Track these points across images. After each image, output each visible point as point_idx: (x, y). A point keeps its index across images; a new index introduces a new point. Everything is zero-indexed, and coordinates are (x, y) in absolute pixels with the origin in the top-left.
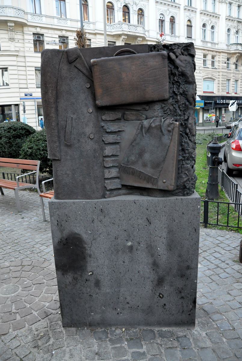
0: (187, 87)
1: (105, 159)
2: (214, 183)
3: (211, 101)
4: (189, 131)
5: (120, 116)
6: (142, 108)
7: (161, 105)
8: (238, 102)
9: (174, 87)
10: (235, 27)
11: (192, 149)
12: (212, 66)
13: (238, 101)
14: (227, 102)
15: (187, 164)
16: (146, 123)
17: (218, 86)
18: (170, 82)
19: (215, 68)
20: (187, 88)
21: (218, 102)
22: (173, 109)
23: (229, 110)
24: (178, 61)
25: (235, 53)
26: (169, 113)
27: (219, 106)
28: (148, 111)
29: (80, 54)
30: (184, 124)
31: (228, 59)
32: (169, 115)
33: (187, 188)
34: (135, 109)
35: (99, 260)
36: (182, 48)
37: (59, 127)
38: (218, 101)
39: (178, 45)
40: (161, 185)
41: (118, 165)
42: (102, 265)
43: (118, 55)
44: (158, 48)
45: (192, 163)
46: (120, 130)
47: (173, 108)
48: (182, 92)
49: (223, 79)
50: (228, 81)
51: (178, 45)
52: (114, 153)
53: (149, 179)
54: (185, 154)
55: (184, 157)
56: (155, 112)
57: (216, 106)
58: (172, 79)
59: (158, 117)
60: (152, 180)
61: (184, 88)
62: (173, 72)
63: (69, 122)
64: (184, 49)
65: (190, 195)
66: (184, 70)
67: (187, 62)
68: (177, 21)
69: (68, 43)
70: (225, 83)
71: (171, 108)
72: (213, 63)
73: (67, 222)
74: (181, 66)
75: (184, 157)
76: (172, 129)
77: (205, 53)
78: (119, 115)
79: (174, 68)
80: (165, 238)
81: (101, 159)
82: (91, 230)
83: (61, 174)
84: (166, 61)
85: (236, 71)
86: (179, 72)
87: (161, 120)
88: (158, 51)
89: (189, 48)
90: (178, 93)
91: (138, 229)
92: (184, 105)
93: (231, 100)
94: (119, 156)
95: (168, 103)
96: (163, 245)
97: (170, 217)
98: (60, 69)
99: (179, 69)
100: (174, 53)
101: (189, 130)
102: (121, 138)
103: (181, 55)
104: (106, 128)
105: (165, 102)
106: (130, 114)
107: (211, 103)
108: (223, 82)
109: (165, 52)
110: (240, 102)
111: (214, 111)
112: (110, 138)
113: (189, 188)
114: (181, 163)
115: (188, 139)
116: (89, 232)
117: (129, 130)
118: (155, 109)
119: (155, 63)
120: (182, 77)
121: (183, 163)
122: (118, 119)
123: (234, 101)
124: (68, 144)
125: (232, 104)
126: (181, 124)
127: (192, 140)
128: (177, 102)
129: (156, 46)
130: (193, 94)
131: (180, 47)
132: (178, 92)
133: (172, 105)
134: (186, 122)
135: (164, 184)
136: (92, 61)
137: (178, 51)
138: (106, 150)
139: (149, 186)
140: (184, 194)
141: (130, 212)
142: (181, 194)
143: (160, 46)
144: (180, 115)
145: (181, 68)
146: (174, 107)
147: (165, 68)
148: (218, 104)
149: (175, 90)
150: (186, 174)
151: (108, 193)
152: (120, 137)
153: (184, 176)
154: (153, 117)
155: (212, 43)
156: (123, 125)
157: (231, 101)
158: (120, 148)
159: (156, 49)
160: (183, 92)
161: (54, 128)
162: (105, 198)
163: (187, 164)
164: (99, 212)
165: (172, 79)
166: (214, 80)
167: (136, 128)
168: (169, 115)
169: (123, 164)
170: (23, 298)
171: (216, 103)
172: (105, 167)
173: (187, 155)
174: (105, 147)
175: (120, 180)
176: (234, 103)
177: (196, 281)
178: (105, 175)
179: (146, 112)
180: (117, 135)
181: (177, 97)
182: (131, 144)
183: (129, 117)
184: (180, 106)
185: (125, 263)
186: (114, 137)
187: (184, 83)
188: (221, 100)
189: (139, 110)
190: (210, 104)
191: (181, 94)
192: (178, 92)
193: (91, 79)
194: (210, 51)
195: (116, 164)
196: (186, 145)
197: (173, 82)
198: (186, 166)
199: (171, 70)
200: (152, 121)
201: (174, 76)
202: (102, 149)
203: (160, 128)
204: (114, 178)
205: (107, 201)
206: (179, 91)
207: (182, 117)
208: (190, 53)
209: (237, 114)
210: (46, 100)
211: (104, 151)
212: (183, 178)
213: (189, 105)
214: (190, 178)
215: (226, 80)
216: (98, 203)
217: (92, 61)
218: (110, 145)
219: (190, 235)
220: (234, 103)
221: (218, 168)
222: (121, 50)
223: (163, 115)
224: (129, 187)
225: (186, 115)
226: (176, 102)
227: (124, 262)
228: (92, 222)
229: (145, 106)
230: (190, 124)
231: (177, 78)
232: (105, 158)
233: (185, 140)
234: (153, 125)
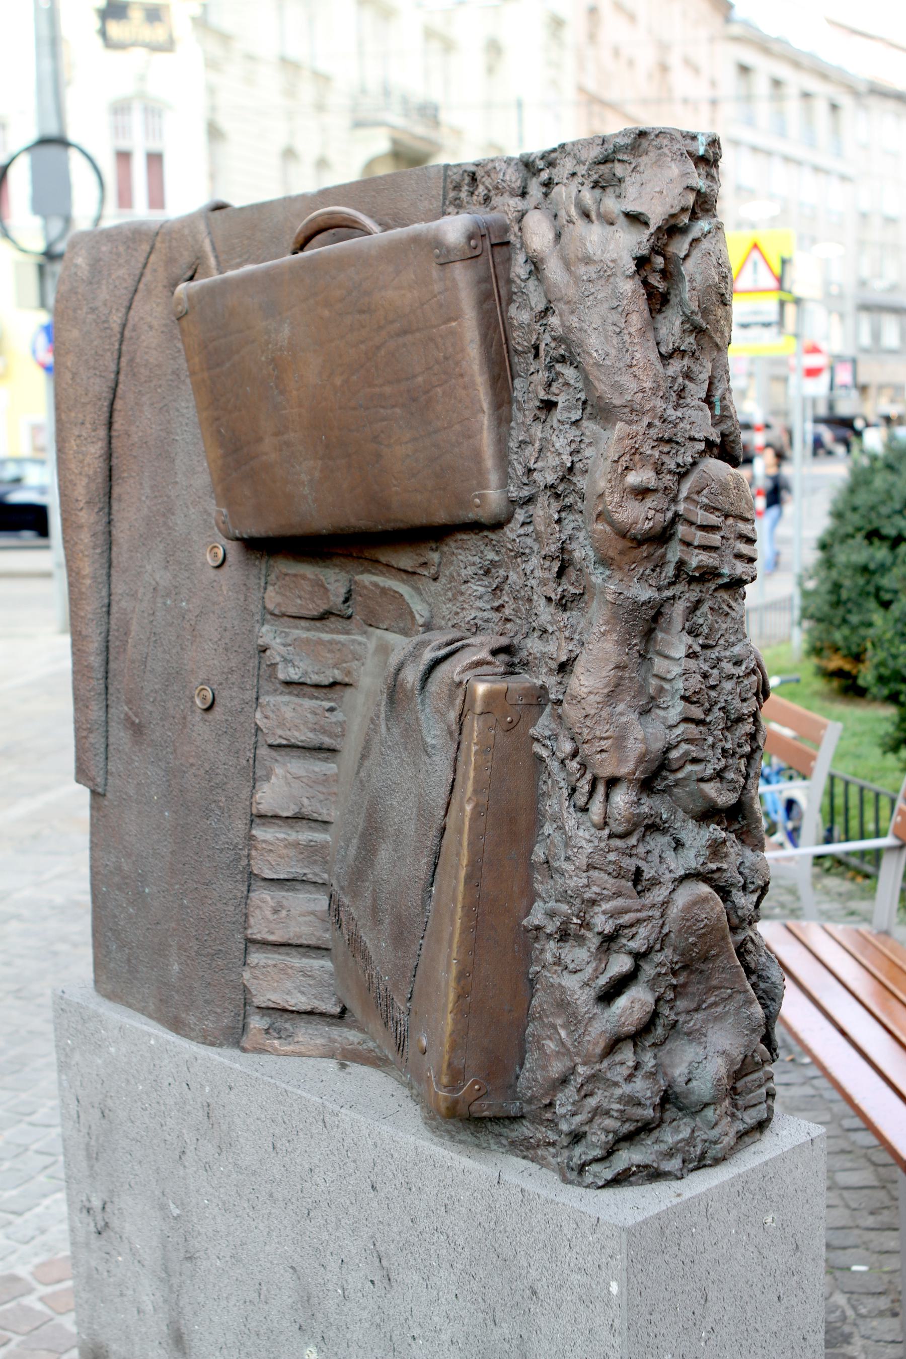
52: (308, 808)
78: (334, 580)
81: (240, 825)
104: (278, 659)
129: (480, 173)
151: (257, 1023)
195: (317, 869)
223: (486, 615)
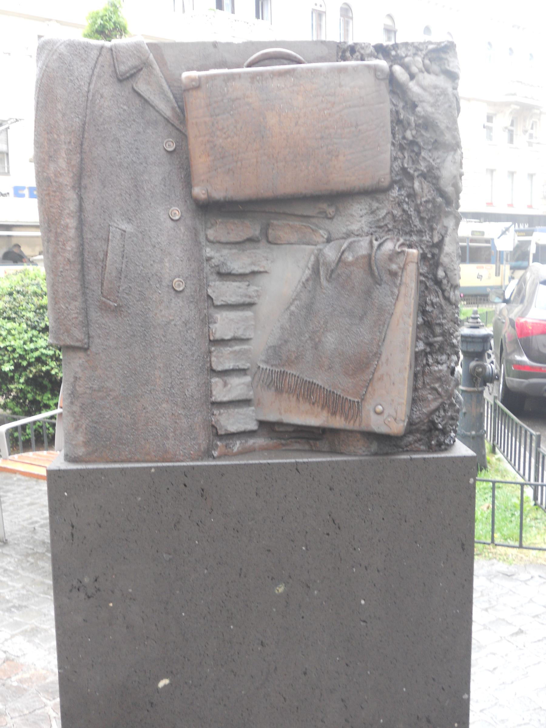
0: (438, 158)
2: (473, 433)
4: (443, 274)
9: (405, 157)
11: (452, 323)
13: (517, 224)
16: (330, 253)
22: (402, 215)
24: (413, 86)
26: (390, 226)
29: (148, 58)
30: (429, 256)
31: (490, 119)
32: (389, 230)
33: (437, 429)
34: (300, 213)
36: (426, 55)
37: (86, 256)
41: (248, 365)
42: (200, 655)
44: (362, 52)
46: (256, 269)
47: (400, 213)
48: (425, 170)
53: (333, 403)
54: (435, 336)
55: (430, 345)
56: (352, 223)
58: (400, 137)
60: (347, 406)
61: (431, 161)
62: (402, 117)
65: (446, 450)
67: (438, 91)
68: (356, 12)
71: (395, 212)
73: (100, 526)
74: (423, 101)
75: (430, 345)
78: (254, 230)
80: (378, 571)
84: (384, 88)
86: (417, 116)
88: (362, 59)
89: (443, 56)
90: (416, 174)
91: (306, 546)
92: (430, 206)
94: (252, 342)
95: (388, 200)
98: (91, 94)
99: (419, 109)
101: (445, 272)
102: (257, 291)
103: (422, 72)
105: (381, 197)
106: (283, 230)
109: (383, 63)
114: (422, 361)
118: (354, 213)
121: (427, 360)
122: (251, 240)
124: (111, 303)
126: (423, 257)
128: (412, 195)
130: (455, 177)
131: (420, 53)
132: (415, 171)
133: (399, 204)
134: (436, 251)
136: (185, 75)
138: (215, 323)
139: (338, 422)
140: (431, 445)
142: (422, 447)
143: (367, 47)
145: (423, 107)
146: (404, 210)
147: (382, 105)
149: (406, 165)
152: (256, 288)
153: (430, 397)
156: (263, 257)
159: (357, 54)
160: (429, 171)
165: (399, 136)
168: (389, 230)
173: (440, 339)
176: (507, 229)
178: (214, 393)
179: (327, 222)
180: (247, 283)
181: (413, 184)
182: (288, 308)
184: (421, 208)
186: (240, 288)
187: (430, 147)
191: (423, 176)
192: (415, 171)
193: (178, 127)
195: (243, 362)
197: (400, 144)
198: (436, 369)
199: (397, 112)
200: (345, 246)
202: (207, 321)
206: (418, 167)
207: (424, 238)
208: (448, 68)
211: (211, 326)
212: (429, 401)
213: (444, 205)
217: (185, 75)
218: (228, 310)
220: (507, 229)
221: (482, 392)
225: (435, 233)
226: (409, 196)
228: (175, 525)
229: (324, 206)
230: (448, 254)
231: (412, 134)
232: (212, 346)
233: (432, 297)
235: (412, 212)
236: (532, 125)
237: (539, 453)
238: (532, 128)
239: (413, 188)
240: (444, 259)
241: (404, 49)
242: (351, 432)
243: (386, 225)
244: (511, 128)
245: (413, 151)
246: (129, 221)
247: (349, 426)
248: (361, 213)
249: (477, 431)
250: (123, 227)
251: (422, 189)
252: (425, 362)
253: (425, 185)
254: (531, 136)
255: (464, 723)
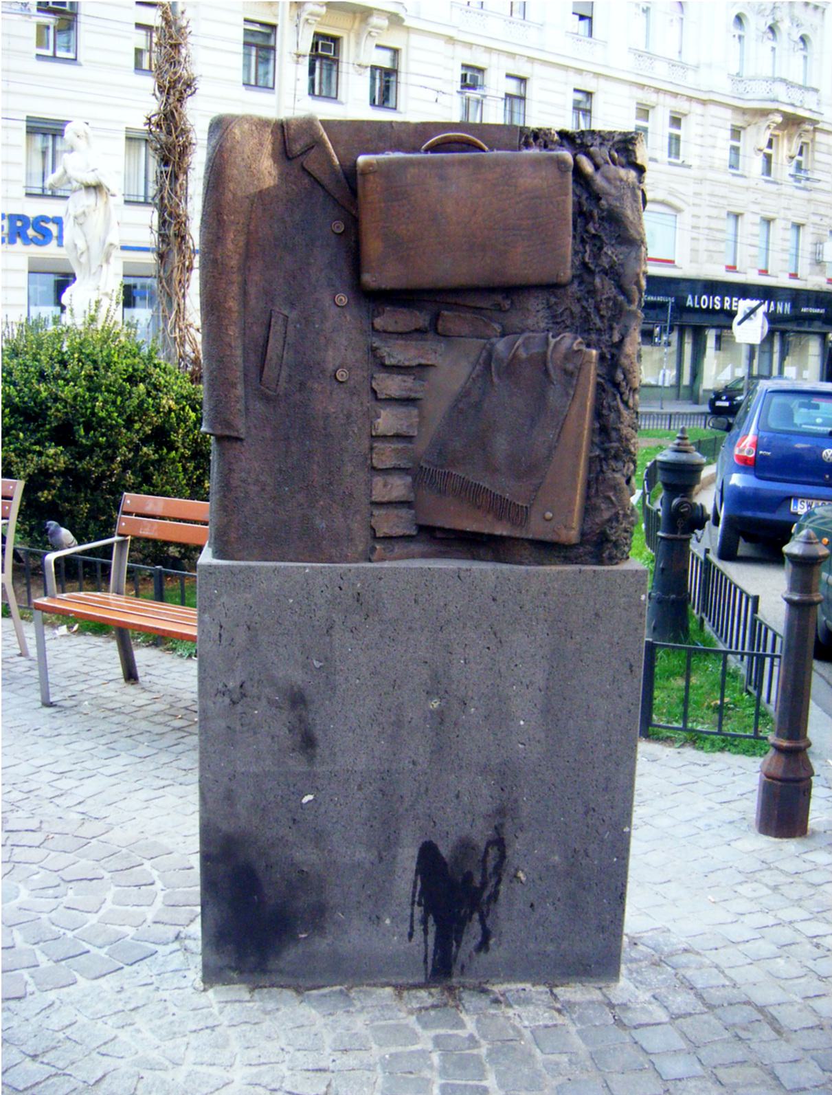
1: (375, 445)
2: (673, 596)
3: (660, 299)
4: (622, 376)
5: (427, 323)
6: (491, 303)
7: (548, 300)
8: (772, 309)
10: (765, 9)
12: (670, 156)
13: (772, 304)
14: (727, 306)
15: (614, 470)
17: (693, 239)
18: (574, 237)
19: (683, 165)
20: (621, 257)
21: (689, 303)
23: (733, 337)
24: (599, 180)
25: (764, 113)
26: (568, 323)
27: (695, 320)
28: (509, 314)
30: (608, 356)
34: (472, 304)
35: (339, 754)
36: (613, 145)
38: (690, 297)
39: (601, 136)
40: (536, 528)
43: (434, 149)
44: (546, 138)
45: (628, 468)
46: (423, 362)
49: (714, 212)
50: (732, 221)
51: (601, 136)
53: (501, 508)
57: (681, 317)
59: (537, 332)
63: (278, 328)
64: (616, 147)
65: (617, 564)
66: (617, 207)
69: (76, 15)
70: (720, 227)
71: (574, 309)
72: (675, 141)
75: (606, 451)
76: (576, 367)
77: (644, 102)
78: (421, 319)
79: (587, 198)
80: (540, 690)
81: (366, 443)
82: (322, 658)
83: (240, 483)
85: (767, 181)
87: (547, 338)
88: (546, 147)
90: (597, 270)
91: (465, 660)
92: (611, 304)
93: (744, 299)
96: (535, 710)
97: (560, 625)
99: (603, 202)
100: (590, 156)
105: (559, 292)
106: (451, 320)
107: (663, 306)
108: (714, 224)
109: (567, 155)
110: (780, 309)
111: (674, 337)
112: (392, 385)
113: (617, 540)
115: (619, 400)
116: (315, 662)
117: (452, 368)
119: (537, 182)
120: (610, 223)
121: (601, 466)
123: (755, 303)
124: (271, 393)
125: (747, 317)
126: (602, 358)
127: (631, 403)
128: (592, 292)
133: (579, 300)
135: (546, 523)
136: (362, 159)
137: (602, 153)
139: (501, 530)
141: (442, 604)
144: (599, 331)
146: (583, 307)
148: (692, 310)
149: (587, 260)
150: (611, 501)
153: (603, 506)
154: (523, 331)
155: (672, 64)
157: (741, 301)
158: (421, 415)
160: (611, 267)
161: (233, 344)
162: (370, 561)
163: (614, 470)
164: (350, 601)
166: (678, 210)
167: (472, 359)
168: (567, 327)
169: (428, 462)
170: (44, 916)
171: (680, 308)
172: (374, 468)
173: (615, 445)
174: (378, 409)
175: (413, 511)
176: (753, 311)
177: (626, 829)
183: (451, 326)
185: (419, 767)
188: (704, 297)
189: (482, 309)
190: (657, 311)
194: (666, 92)
196: (613, 416)
201: (585, 219)
202: (371, 417)
203: (542, 363)
204: (396, 503)
205: (377, 569)
206: (600, 262)
209: (766, 356)
210: (215, 261)
214: (621, 512)
215: (724, 215)
216: (350, 574)
217: (362, 159)
219: (614, 681)
220: (753, 311)
221: (687, 541)
222: (445, 137)
224: (439, 535)
226: (588, 292)
227: (414, 763)
229: (498, 298)
234: (523, 354)
235: (591, 310)
236: (801, 148)
237: (755, 621)
238: (800, 154)
239: (592, 283)
240: (625, 361)
241: (590, 138)
242: (517, 539)
243: (563, 321)
244: (768, 151)
245: (595, 245)
246: (292, 306)
247: (517, 533)
248: (538, 308)
249: (678, 594)
250: (286, 312)
251: (603, 285)
252: (599, 468)
253: (607, 281)
254: (799, 164)
255: (624, 859)
